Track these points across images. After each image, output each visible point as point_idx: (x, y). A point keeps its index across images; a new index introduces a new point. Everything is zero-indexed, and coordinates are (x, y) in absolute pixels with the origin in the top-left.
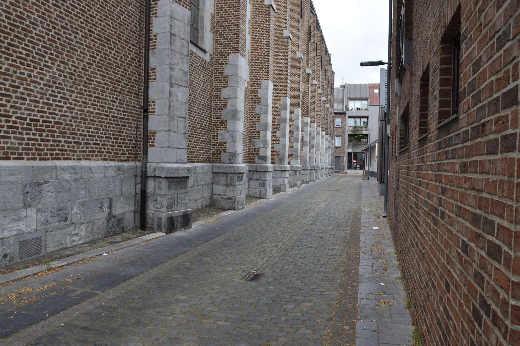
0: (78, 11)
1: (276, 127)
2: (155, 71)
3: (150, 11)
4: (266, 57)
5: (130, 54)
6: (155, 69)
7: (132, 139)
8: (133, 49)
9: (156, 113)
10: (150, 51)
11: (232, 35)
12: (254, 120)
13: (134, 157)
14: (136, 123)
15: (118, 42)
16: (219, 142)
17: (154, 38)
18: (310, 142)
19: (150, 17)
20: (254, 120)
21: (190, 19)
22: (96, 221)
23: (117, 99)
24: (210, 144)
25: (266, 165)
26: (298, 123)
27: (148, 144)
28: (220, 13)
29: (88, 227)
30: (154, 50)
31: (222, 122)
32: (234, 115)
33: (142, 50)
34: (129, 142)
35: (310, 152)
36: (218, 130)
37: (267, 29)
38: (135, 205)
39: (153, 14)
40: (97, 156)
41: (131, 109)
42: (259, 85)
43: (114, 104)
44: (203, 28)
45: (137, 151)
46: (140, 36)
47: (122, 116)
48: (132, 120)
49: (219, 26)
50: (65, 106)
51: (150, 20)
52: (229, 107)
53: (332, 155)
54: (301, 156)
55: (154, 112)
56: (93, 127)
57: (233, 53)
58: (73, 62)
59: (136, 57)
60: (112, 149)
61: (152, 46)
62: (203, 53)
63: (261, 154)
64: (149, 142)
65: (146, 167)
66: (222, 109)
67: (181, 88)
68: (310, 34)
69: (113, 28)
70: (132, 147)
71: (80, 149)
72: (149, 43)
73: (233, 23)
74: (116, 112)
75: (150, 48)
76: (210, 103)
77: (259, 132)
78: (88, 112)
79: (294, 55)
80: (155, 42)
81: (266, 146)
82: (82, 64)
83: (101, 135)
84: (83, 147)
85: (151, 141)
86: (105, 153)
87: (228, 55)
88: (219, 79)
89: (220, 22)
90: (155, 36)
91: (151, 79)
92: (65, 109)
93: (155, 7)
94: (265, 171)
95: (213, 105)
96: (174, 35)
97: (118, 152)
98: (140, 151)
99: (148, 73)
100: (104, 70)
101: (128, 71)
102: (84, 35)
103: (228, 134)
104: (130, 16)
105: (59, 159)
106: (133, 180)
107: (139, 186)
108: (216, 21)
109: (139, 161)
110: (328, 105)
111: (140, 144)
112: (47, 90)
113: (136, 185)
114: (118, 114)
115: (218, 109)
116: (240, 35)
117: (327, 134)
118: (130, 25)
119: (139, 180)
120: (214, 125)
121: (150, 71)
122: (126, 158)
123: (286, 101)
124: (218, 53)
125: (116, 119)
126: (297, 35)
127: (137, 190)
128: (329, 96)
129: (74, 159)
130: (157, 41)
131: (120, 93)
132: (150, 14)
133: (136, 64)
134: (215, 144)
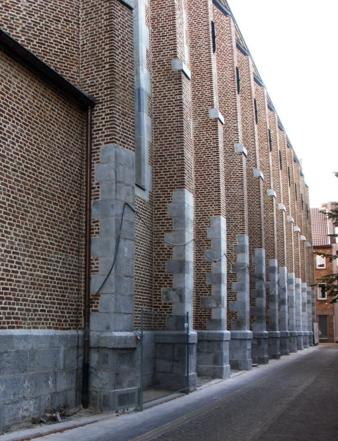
0: (31, 171)
1: (231, 277)
2: (99, 223)
3: (91, 157)
4: (216, 185)
5: (72, 207)
6: (98, 221)
7: (74, 303)
8: (75, 200)
9: (100, 273)
10: (92, 201)
11: (175, 167)
12: (203, 269)
13: (75, 325)
14: (77, 284)
15: (61, 196)
16: (163, 302)
17: (96, 186)
18: (279, 295)
19: (91, 163)
20: (203, 269)
21: (135, 162)
22: (43, 397)
23: (60, 258)
24: (151, 306)
25: (221, 332)
26: (261, 268)
27: (91, 309)
28: (159, 139)
29: (36, 403)
30: (97, 200)
31: (166, 277)
32: (182, 266)
33: (82, 200)
34: (71, 307)
35: (279, 310)
36: (161, 286)
37: (215, 149)
38: (77, 381)
39: (94, 160)
40: (43, 323)
41: (73, 269)
42: (208, 223)
43: (58, 264)
44: (141, 160)
45: (78, 317)
46: (81, 185)
47: (65, 278)
48: (74, 281)
49: (158, 156)
50: (19, 271)
51: (91, 167)
52: (174, 257)
53: (313, 313)
54: (267, 317)
55: (97, 271)
56: (40, 292)
57: (177, 188)
58: (26, 224)
59: (77, 209)
60: (56, 316)
61: (94, 195)
62: (142, 191)
63: (214, 316)
64: (92, 306)
65: (89, 337)
66: (166, 260)
67: (127, 241)
68: (270, 141)
69: (58, 181)
70: (74, 313)
71: (30, 317)
72: (91, 192)
73: (176, 152)
74: (60, 273)
75: (92, 197)
76: (150, 253)
77: (210, 286)
78: (37, 275)
79: (250, 174)
80: (98, 191)
81: (220, 306)
82: (33, 224)
83: (47, 301)
84: (32, 315)
85: (94, 305)
86: (50, 321)
87: (171, 191)
88: (161, 221)
89: (159, 151)
90: (98, 184)
91: (93, 233)
92: (19, 275)
93: (96, 152)
94: (220, 340)
95: (154, 255)
96: (120, 182)
97: (61, 319)
98: (81, 317)
99: (90, 226)
100: (50, 228)
101: (70, 226)
102: (34, 194)
103: (174, 293)
104: (72, 166)
105: (13, 328)
106: (75, 352)
107: (81, 358)
108: (154, 149)
109: (80, 329)
110: (303, 238)
111: (81, 309)
112: (7, 256)
113: (77, 358)
114: (61, 276)
115: (161, 260)
116: (186, 166)
117: (304, 281)
118: (72, 175)
119: (81, 351)
120: (155, 281)
121: (92, 224)
122: (68, 326)
123: (244, 241)
124: (159, 189)
125: (59, 281)
126: (253, 146)
127: (79, 363)
128: (303, 223)
129: (25, 328)
130: (100, 190)
131: (63, 251)
132: (91, 160)
133: (77, 217)
134: (157, 305)
